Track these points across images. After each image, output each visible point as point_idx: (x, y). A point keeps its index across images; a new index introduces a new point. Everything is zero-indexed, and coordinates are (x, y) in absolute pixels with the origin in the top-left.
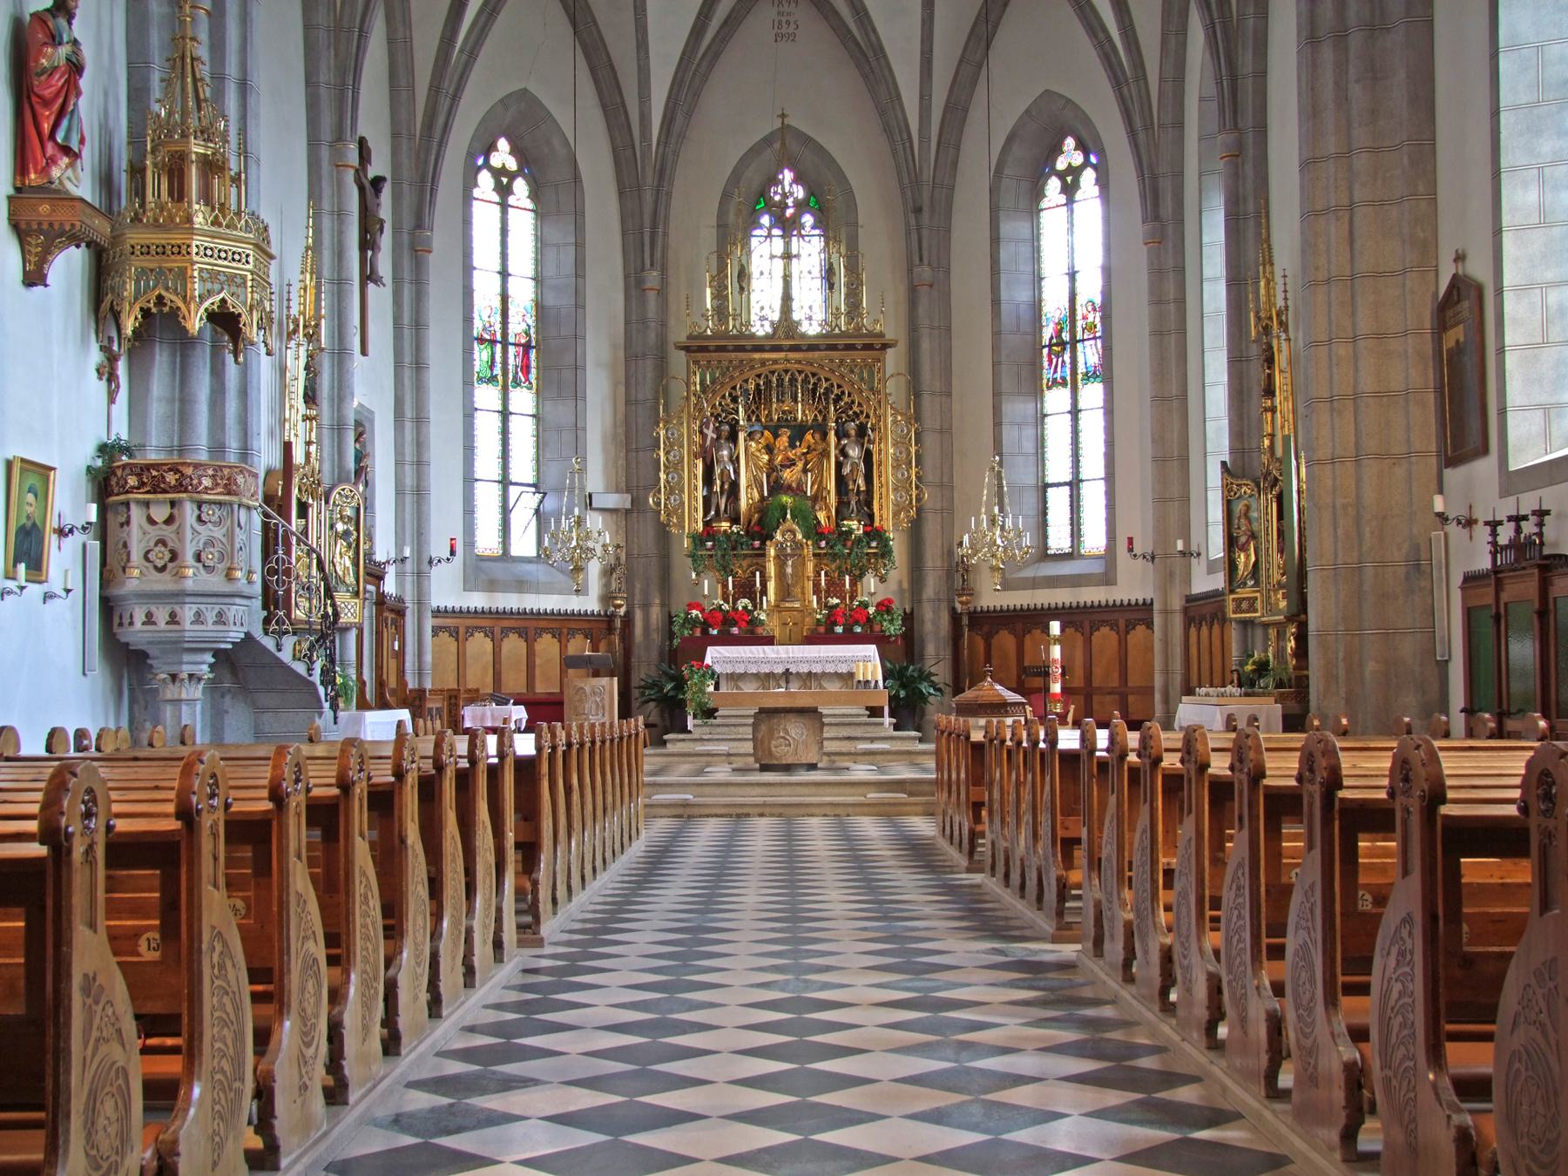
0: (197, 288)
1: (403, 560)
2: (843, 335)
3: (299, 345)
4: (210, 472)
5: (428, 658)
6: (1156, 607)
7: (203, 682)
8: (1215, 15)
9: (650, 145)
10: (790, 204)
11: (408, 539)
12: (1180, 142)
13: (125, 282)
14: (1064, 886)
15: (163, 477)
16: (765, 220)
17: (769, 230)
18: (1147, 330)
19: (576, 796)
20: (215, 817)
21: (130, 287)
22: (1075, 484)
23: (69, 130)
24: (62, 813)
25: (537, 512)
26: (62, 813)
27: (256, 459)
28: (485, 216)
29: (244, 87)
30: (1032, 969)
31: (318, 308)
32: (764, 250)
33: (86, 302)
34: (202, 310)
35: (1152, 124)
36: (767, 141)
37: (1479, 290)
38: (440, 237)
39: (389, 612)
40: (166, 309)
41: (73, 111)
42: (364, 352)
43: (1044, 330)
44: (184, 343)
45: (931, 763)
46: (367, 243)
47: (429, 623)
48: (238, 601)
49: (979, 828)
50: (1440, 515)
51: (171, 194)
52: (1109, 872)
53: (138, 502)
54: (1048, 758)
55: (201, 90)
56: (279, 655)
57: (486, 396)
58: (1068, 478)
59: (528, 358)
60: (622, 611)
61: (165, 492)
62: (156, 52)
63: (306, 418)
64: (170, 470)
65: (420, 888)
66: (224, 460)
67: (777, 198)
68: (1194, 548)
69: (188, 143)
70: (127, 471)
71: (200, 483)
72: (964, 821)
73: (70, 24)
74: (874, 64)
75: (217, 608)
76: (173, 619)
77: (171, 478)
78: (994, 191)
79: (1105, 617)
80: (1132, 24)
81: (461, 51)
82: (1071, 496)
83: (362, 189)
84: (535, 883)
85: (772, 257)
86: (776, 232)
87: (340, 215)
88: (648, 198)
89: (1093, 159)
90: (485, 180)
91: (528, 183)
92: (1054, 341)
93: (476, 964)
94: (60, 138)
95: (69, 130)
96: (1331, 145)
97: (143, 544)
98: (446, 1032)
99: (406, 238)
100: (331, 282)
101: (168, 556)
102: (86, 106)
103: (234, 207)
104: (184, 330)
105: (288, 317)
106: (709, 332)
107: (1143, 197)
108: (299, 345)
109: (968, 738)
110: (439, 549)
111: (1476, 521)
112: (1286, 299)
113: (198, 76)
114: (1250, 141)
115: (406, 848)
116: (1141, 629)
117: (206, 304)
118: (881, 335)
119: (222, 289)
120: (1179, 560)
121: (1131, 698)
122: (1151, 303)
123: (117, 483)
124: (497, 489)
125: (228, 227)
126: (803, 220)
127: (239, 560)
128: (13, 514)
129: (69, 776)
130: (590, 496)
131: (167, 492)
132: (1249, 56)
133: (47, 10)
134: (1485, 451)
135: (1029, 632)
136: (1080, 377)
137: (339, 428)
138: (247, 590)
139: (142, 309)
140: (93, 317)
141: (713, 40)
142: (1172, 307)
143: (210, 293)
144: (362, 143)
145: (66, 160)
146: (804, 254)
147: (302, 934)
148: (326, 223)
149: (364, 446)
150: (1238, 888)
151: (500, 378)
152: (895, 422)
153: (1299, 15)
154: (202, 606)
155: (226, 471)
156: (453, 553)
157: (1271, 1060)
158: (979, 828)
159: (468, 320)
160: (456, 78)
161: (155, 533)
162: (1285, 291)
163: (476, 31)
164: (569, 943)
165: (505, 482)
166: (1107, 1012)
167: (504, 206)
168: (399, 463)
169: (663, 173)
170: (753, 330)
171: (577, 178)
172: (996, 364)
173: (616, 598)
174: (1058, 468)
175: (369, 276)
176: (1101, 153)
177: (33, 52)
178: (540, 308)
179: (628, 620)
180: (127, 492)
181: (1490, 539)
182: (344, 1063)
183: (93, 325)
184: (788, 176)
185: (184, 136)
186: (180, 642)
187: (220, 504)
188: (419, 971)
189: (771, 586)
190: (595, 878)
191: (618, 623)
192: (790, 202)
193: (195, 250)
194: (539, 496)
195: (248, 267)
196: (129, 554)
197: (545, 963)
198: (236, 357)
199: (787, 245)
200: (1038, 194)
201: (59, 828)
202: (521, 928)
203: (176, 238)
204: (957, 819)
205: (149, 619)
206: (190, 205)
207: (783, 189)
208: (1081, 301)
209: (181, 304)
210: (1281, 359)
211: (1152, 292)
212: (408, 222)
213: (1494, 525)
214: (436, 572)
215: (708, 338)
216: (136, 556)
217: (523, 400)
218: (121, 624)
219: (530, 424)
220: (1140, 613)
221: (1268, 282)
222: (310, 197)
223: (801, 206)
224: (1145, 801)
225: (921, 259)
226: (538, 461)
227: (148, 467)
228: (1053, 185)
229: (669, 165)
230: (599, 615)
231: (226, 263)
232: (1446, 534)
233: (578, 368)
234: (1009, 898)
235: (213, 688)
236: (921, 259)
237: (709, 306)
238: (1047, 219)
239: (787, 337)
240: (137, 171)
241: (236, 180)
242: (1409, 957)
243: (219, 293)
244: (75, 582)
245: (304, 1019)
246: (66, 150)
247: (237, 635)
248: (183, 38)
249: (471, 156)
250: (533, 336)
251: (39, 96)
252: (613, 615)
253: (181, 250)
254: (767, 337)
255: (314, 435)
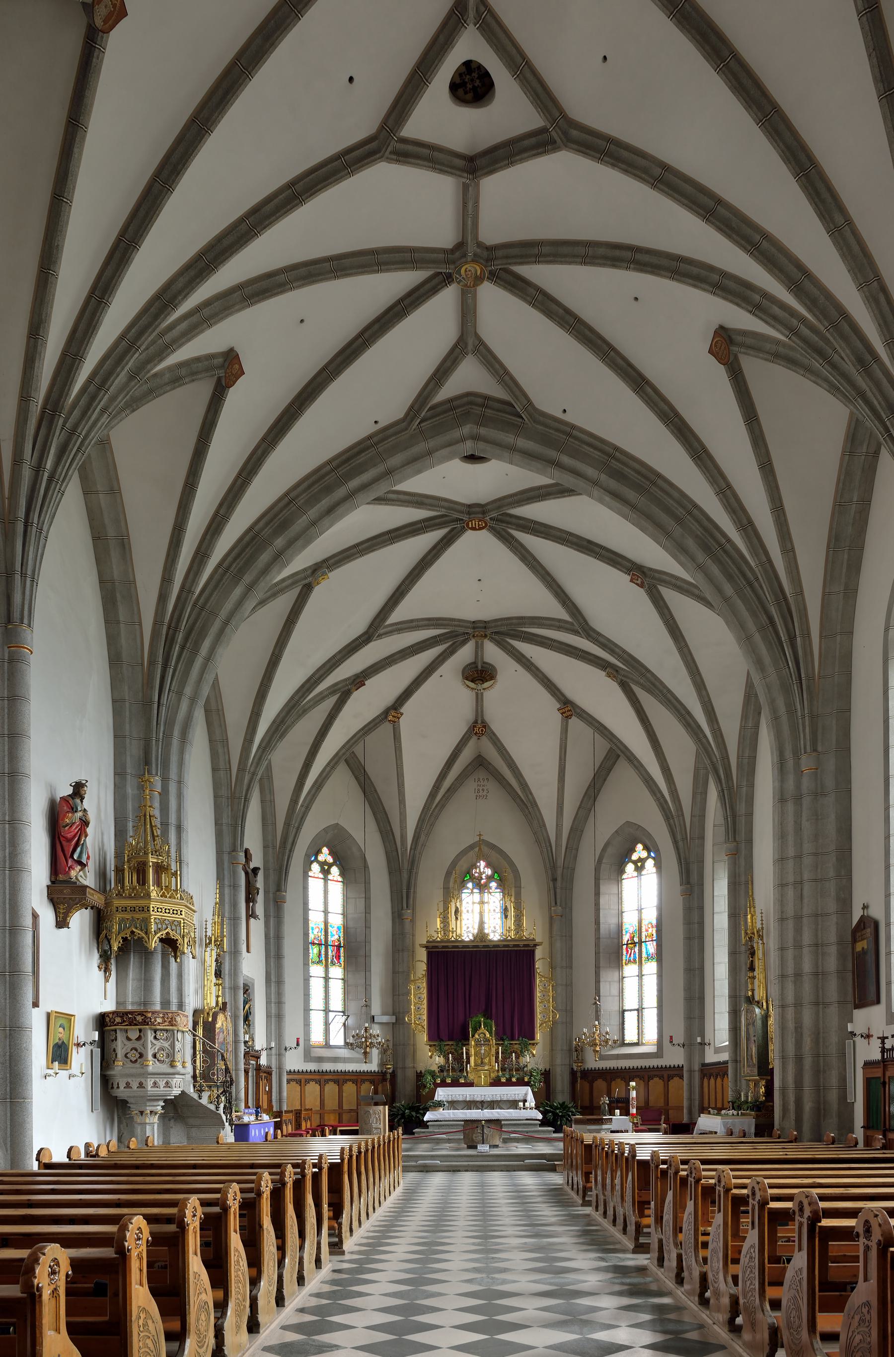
0: (153, 927)
1: (270, 1049)
2: (512, 940)
3: (212, 950)
4: (161, 1015)
5: (285, 1094)
6: (685, 1069)
7: (158, 1115)
8: (724, 786)
9: (406, 850)
10: (484, 877)
11: (273, 1038)
12: (702, 846)
13: (113, 925)
14: (640, 1226)
15: (135, 1018)
16: (470, 885)
17: (472, 891)
18: (681, 937)
19: (363, 1177)
20: (140, 1250)
21: (116, 928)
22: (640, 1010)
23: (81, 853)
24: (36, 1277)
25: (344, 1024)
26: (36, 1277)
27: (187, 1007)
28: (315, 885)
29: (179, 828)
30: (621, 1271)
31: (222, 932)
32: (469, 899)
33: (93, 928)
34: (156, 938)
35: (687, 838)
36: (471, 847)
37: (876, 924)
38: (291, 894)
39: (262, 1074)
40: (136, 938)
41: (83, 844)
42: (248, 951)
43: (624, 936)
44: (146, 954)
45: (561, 1145)
46: (250, 898)
47: (285, 1078)
48: (177, 1076)
49: (589, 1185)
50: (852, 1033)
51: (138, 882)
52: (668, 1229)
53: (121, 1030)
54: (630, 1163)
55: (155, 831)
56: (200, 1101)
57: (317, 971)
58: (636, 1007)
59: (339, 952)
60: (390, 1071)
61: (136, 1025)
62: (131, 813)
63: (216, 985)
64: (139, 1014)
65: (271, 1248)
66: (169, 1009)
67: (476, 875)
68: (707, 1041)
69: (148, 858)
70: (115, 1015)
71: (156, 1021)
72: (579, 1179)
73: (82, 802)
74: (531, 810)
75: (165, 1080)
76: (141, 1085)
77: (139, 1018)
78: (597, 870)
79: (657, 1073)
80: (676, 789)
81: (302, 806)
82: (638, 1016)
83: (247, 873)
84: (340, 1225)
85: (474, 903)
86: (475, 891)
87: (234, 887)
88: (405, 875)
89: (652, 854)
90: (315, 867)
91: (339, 869)
92: (630, 942)
93: (305, 1275)
94: (75, 857)
95: (81, 853)
96: (791, 852)
97: (124, 1050)
98: (288, 1314)
99: (271, 895)
100: (230, 919)
101: (138, 1055)
102: (91, 840)
103: (173, 887)
104: (146, 949)
105: (206, 936)
106: (439, 939)
107: (681, 873)
108: (212, 950)
109: (582, 1142)
110: (290, 1042)
111: (872, 1036)
112: (762, 924)
113: (153, 824)
114: (743, 847)
115: (263, 1230)
116: (676, 1079)
117: (158, 935)
118: (534, 940)
119: (167, 928)
120: (698, 1047)
121: (671, 1112)
122: (684, 924)
123: (110, 1021)
124: (322, 1014)
125: (170, 897)
126: (491, 885)
127: (178, 1057)
128: (51, 1038)
129: (41, 1255)
130: (373, 1017)
131: (137, 1025)
132: (743, 805)
133: (69, 795)
134: (878, 1002)
135: (614, 1080)
136: (643, 959)
137: (234, 989)
138: (182, 1071)
139: (122, 938)
140: (95, 941)
141: (441, 799)
142: (696, 926)
143: (160, 930)
144: (247, 852)
145: (79, 867)
146: (491, 901)
147: (198, 1292)
148: (227, 891)
149: (249, 995)
150: (751, 1258)
151: (324, 961)
152: (541, 981)
153: (774, 788)
154: (157, 1080)
155: (170, 1015)
156: (298, 1044)
157: (771, 1349)
158: (589, 1185)
159: (306, 934)
160: (299, 819)
161: (130, 1045)
162: (762, 920)
163: (309, 797)
164: (359, 1253)
165: (327, 1011)
166: (666, 1300)
167: (326, 880)
168: (268, 1003)
169: (413, 863)
170: (463, 938)
171: (366, 866)
172: (597, 953)
173: (387, 1065)
174: (631, 1001)
175: (251, 915)
176: (657, 851)
177: (61, 816)
178: (346, 929)
179: (393, 1075)
180: (115, 1025)
181: (881, 1045)
182: (224, 1348)
183: (96, 945)
184: (482, 864)
185: (146, 853)
186: (144, 1097)
187: (167, 1031)
188: (271, 1288)
189: (472, 1059)
190: (374, 1212)
191: (388, 1076)
192: (484, 876)
193: (152, 909)
194: (345, 1017)
195: (181, 916)
196: (116, 1054)
197: (346, 1266)
198: (176, 961)
199: (481, 898)
200: (622, 871)
201: (33, 1286)
202: (331, 1245)
203: (141, 902)
204: (575, 1179)
205: (128, 1085)
206: (149, 887)
207: (480, 870)
208: (644, 923)
209: (144, 935)
210: (759, 954)
211: (684, 918)
212: (272, 888)
213: (883, 1039)
214: (288, 1054)
215: (438, 942)
216: (120, 1053)
217: (337, 972)
218: (112, 1088)
219: (340, 984)
220: (675, 1072)
221: (752, 916)
222: (218, 878)
223: (490, 878)
224: (691, 1199)
225: (556, 903)
226: (344, 1001)
227: (127, 1013)
228: (630, 868)
229: (417, 859)
230: (378, 1072)
231: (169, 915)
232: (854, 1041)
233: (367, 956)
234: (606, 1224)
235: (163, 1117)
236: (556, 903)
237: (439, 927)
238: (625, 883)
239: (481, 941)
240: (119, 871)
241: (175, 874)
242: (867, 1324)
243: (165, 929)
244: (86, 1068)
245: (199, 1334)
246: (80, 863)
247: (176, 1092)
248: (145, 806)
249: (308, 856)
250: (342, 941)
251: (64, 837)
252: (386, 1073)
253: (145, 909)
254: (471, 941)
255: (220, 992)
